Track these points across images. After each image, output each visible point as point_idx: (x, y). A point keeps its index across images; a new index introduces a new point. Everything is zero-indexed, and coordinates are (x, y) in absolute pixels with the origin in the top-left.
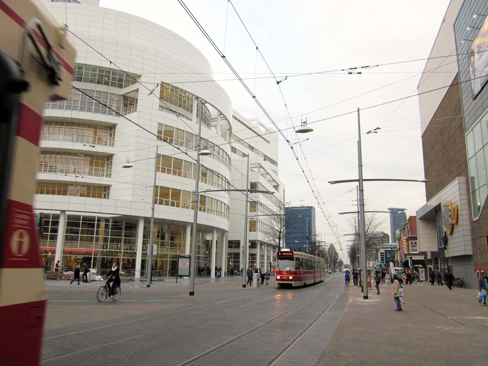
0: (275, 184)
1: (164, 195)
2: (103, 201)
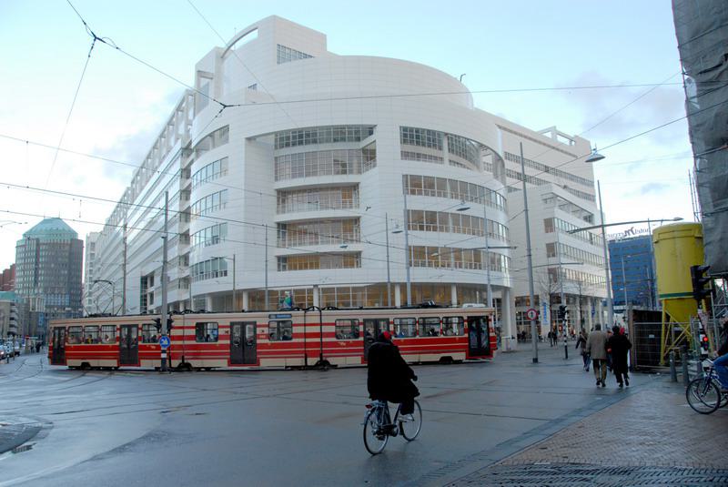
0: (585, 214)
1: (419, 255)
2: (354, 271)
